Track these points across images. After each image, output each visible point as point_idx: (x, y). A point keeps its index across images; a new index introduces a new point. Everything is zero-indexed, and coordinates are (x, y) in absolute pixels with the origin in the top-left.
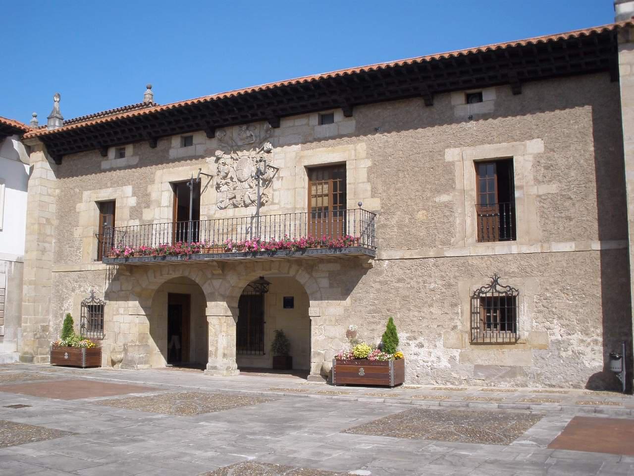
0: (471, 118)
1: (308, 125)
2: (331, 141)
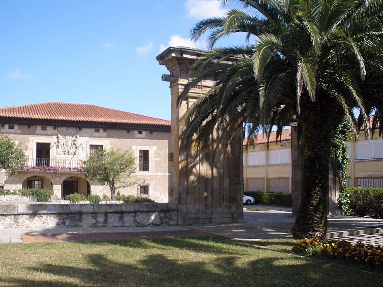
0: (139, 138)
1: (91, 131)
2: (99, 138)
